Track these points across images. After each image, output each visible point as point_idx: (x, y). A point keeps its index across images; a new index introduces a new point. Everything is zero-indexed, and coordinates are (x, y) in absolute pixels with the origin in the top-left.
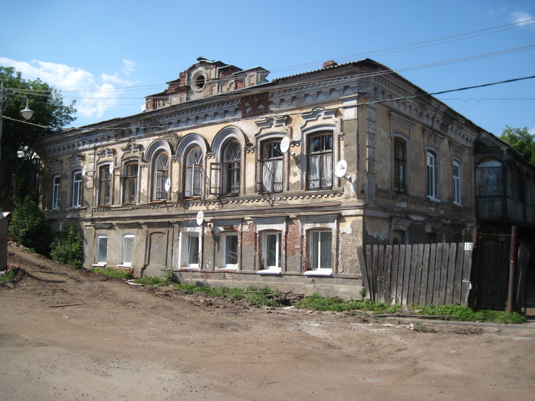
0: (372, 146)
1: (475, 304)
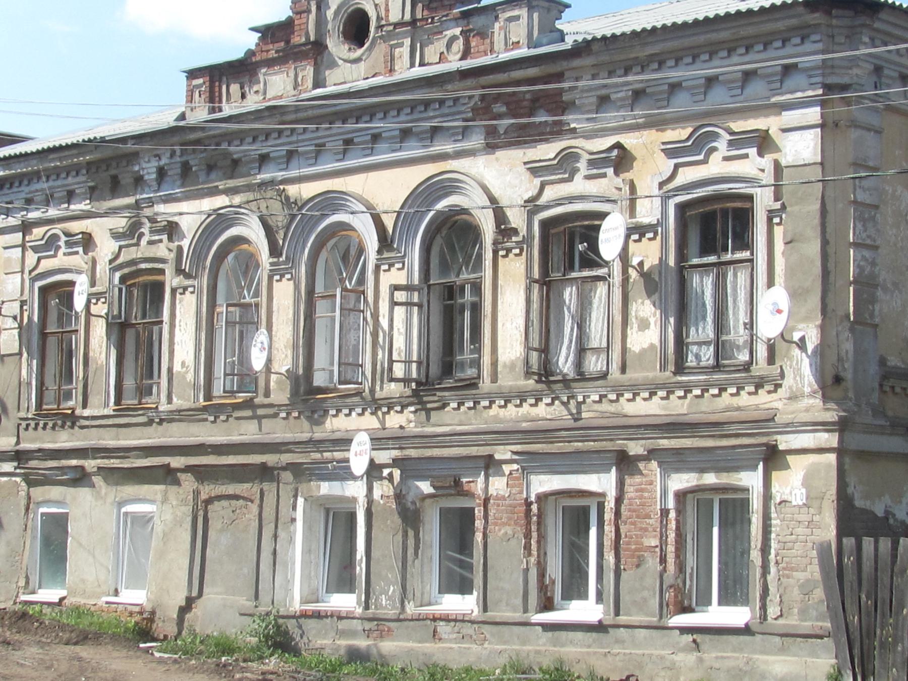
0: (868, 242)
1: (835, 562)
